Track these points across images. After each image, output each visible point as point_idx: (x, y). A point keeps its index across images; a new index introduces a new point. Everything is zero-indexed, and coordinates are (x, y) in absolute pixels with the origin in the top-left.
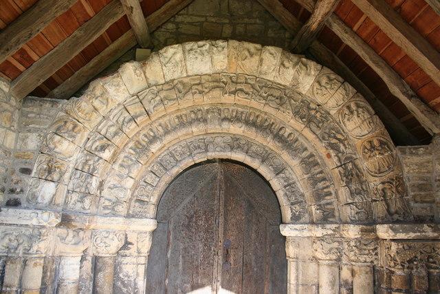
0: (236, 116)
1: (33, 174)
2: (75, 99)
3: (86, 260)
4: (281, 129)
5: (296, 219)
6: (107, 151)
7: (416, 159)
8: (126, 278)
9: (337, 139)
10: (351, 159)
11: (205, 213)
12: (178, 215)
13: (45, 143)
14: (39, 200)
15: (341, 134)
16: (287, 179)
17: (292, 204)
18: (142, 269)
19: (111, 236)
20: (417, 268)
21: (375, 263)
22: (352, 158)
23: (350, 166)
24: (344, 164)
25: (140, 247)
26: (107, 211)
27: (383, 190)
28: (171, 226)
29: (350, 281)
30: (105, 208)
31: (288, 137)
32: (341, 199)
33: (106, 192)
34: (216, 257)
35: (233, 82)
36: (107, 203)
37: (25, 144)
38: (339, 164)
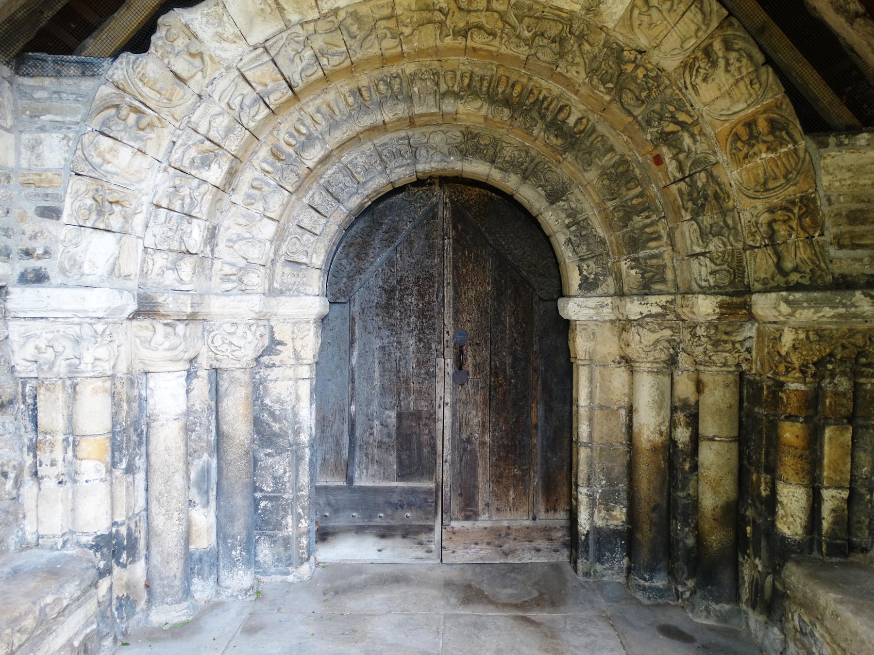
0: (469, 85)
1: (65, 218)
2: (133, 57)
3: (197, 377)
4: (561, 109)
5: (588, 286)
6: (214, 166)
7: (848, 158)
8: (277, 406)
9: (677, 123)
10: (704, 164)
11: (416, 283)
12: (368, 288)
13: (79, 152)
14: (86, 268)
15: (688, 113)
16: (572, 214)
17: (582, 260)
18: (305, 389)
19: (240, 332)
20: (833, 375)
21: (745, 367)
22: (706, 161)
23: (701, 179)
24: (690, 176)
25: (298, 349)
26: (229, 286)
27: (770, 224)
28: (356, 309)
29: (692, 400)
30: (226, 278)
31: (576, 124)
32: (679, 245)
33: (222, 248)
34: (441, 361)
35: (460, 9)
36: (227, 270)
37: (38, 157)
38: (679, 176)
